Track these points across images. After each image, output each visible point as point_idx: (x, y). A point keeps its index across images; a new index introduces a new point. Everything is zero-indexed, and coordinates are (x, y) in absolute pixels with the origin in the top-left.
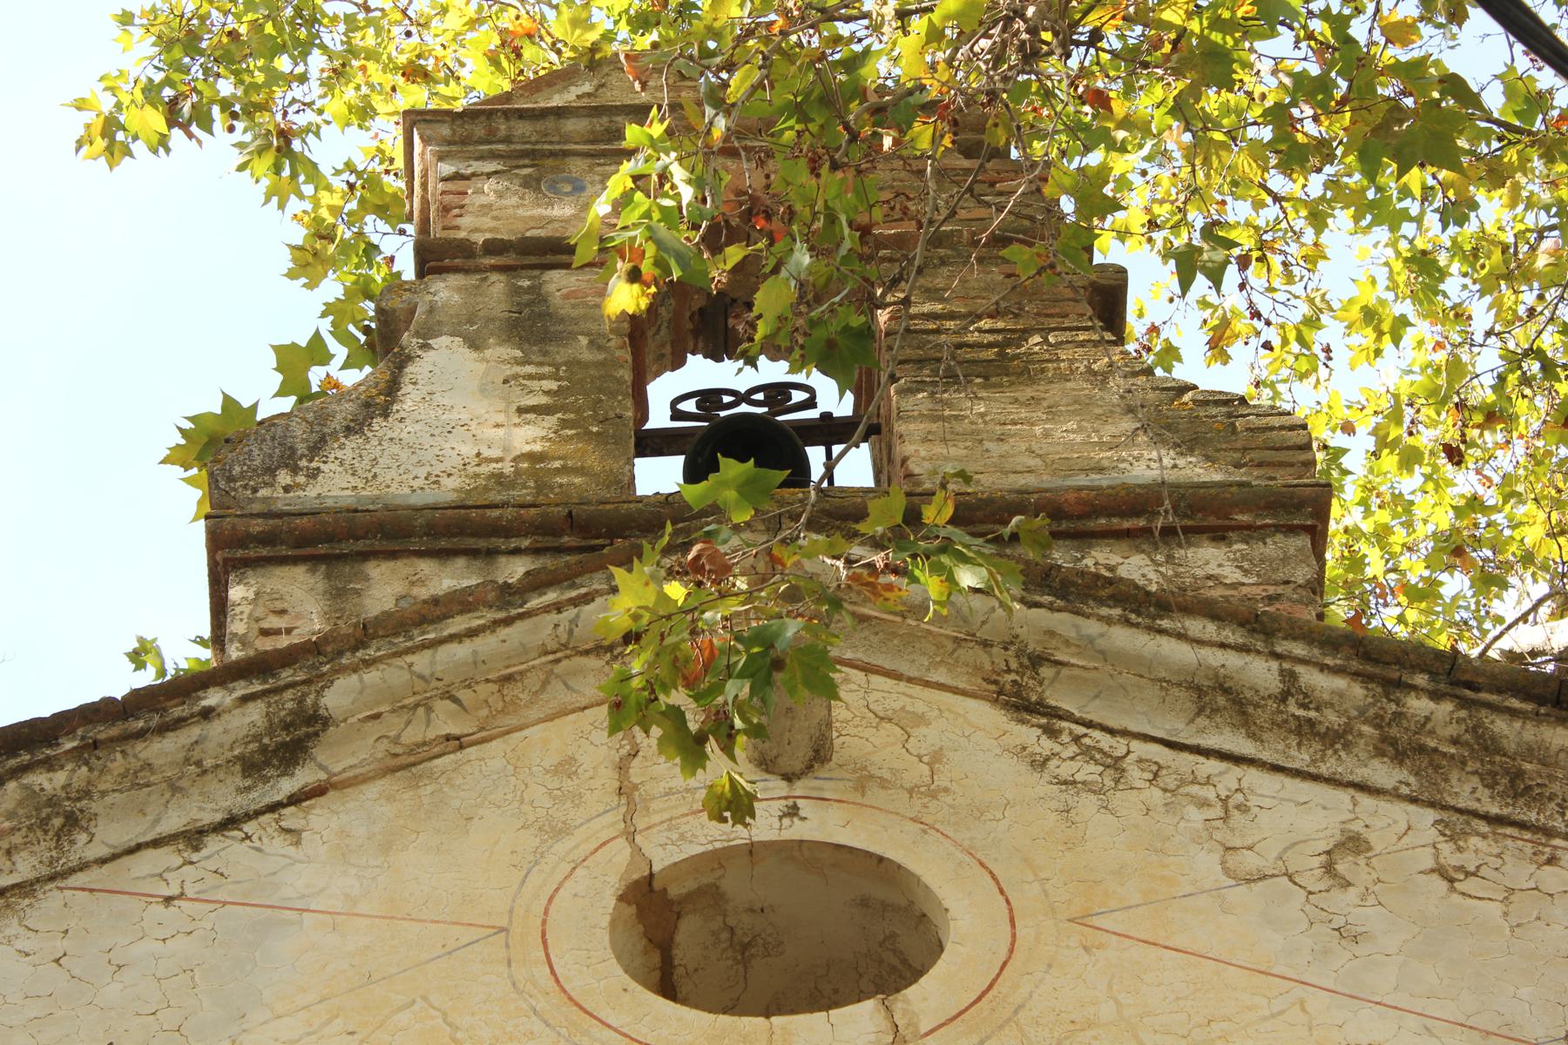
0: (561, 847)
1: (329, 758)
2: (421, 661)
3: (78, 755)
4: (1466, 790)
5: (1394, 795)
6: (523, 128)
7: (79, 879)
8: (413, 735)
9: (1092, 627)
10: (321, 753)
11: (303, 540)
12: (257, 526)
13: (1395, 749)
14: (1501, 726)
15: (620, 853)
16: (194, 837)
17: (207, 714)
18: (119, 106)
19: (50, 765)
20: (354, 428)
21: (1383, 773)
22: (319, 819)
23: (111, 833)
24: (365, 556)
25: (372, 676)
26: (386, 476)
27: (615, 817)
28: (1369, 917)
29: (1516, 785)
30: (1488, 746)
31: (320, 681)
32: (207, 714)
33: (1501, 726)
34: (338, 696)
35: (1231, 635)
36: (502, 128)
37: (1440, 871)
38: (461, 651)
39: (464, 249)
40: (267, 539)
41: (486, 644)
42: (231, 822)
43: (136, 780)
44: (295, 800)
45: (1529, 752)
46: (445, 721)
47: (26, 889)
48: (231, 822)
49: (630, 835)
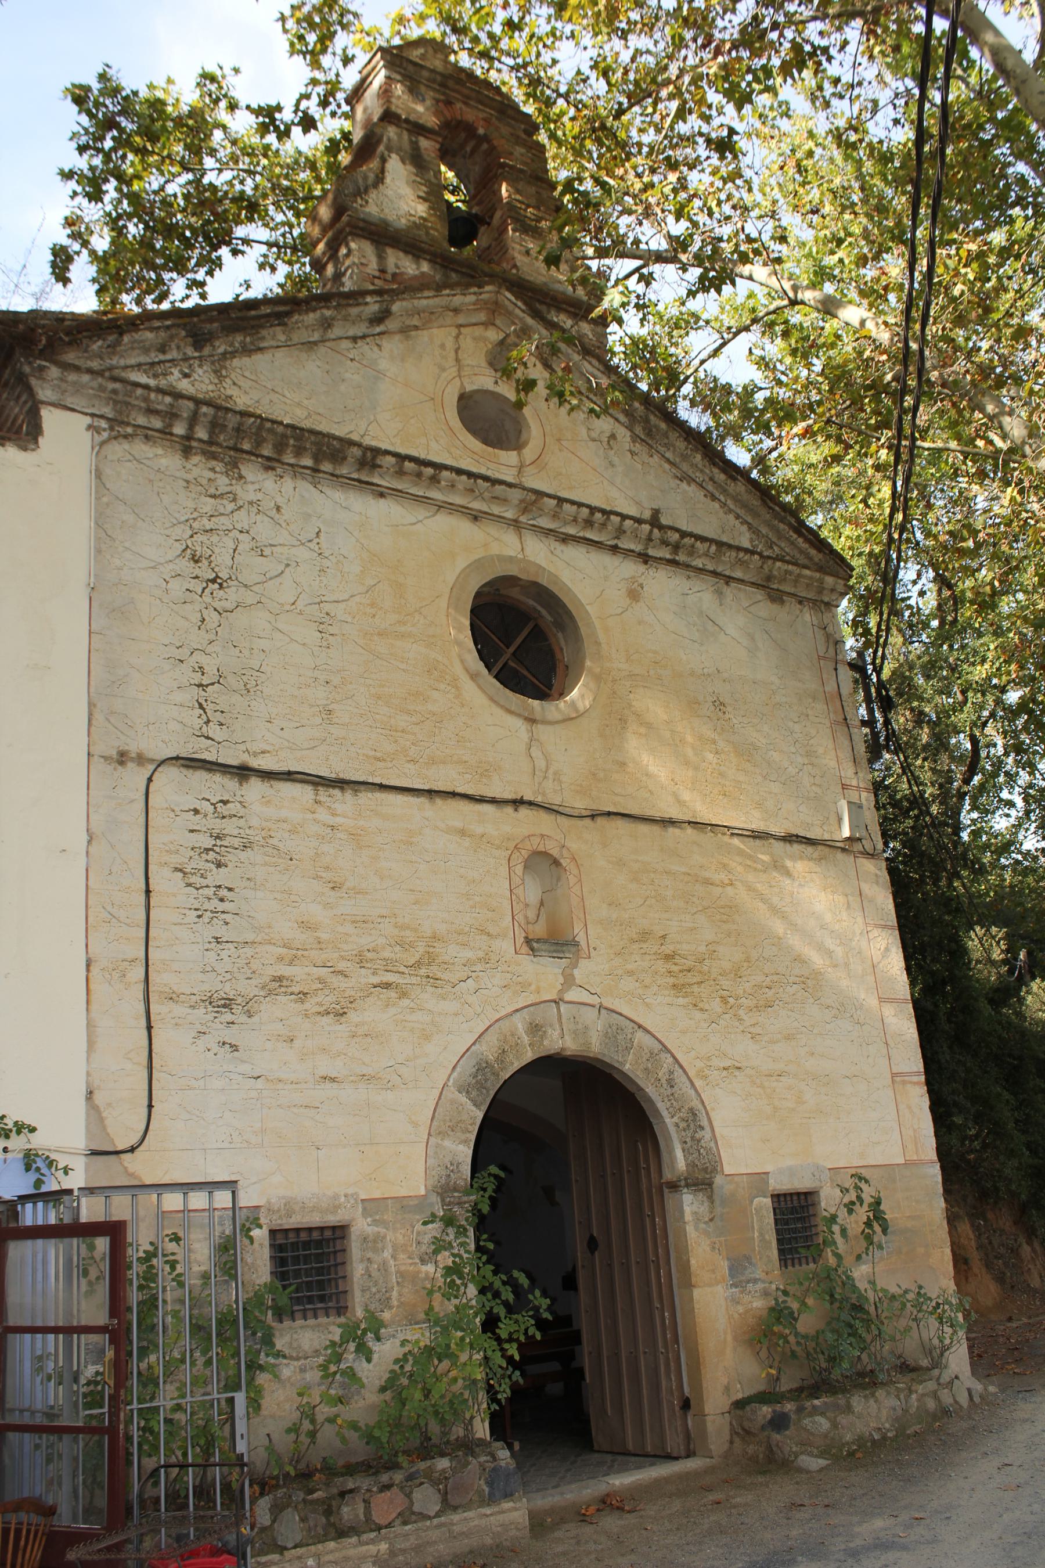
0: (444, 375)
1: (391, 324)
2: (416, 302)
3: (335, 308)
4: (638, 430)
5: (623, 424)
6: (411, 68)
7: (328, 344)
8: (408, 323)
9: (570, 351)
10: (387, 322)
11: (371, 233)
12: (361, 224)
13: (627, 413)
14: (652, 417)
15: (457, 382)
16: (354, 339)
17: (366, 304)
18: (624, 305)
19: (328, 308)
20: (375, 186)
21: (622, 418)
22: (385, 342)
23: (336, 331)
24: (387, 244)
25: (404, 303)
26: (386, 211)
27: (455, 369)
28: (616, 460)
29: (649, 433)
30: (647, 421)
31: (393, 301)
32: (366, 304)
33: (652, 417)
34: (395, 307)
35: (602, 368)
36: (405, 64)
37: (630, 451)
38: (425, 302)
39: (397, 117)
40: (362, 229)
41: (431, 302)
42: (364, 337)
43: (345, 319)
44: (379, 334)
45: (655, 426)
46: (415, 321)
47: (315, 343)
48: (364, 337)
49: (460, 376)
